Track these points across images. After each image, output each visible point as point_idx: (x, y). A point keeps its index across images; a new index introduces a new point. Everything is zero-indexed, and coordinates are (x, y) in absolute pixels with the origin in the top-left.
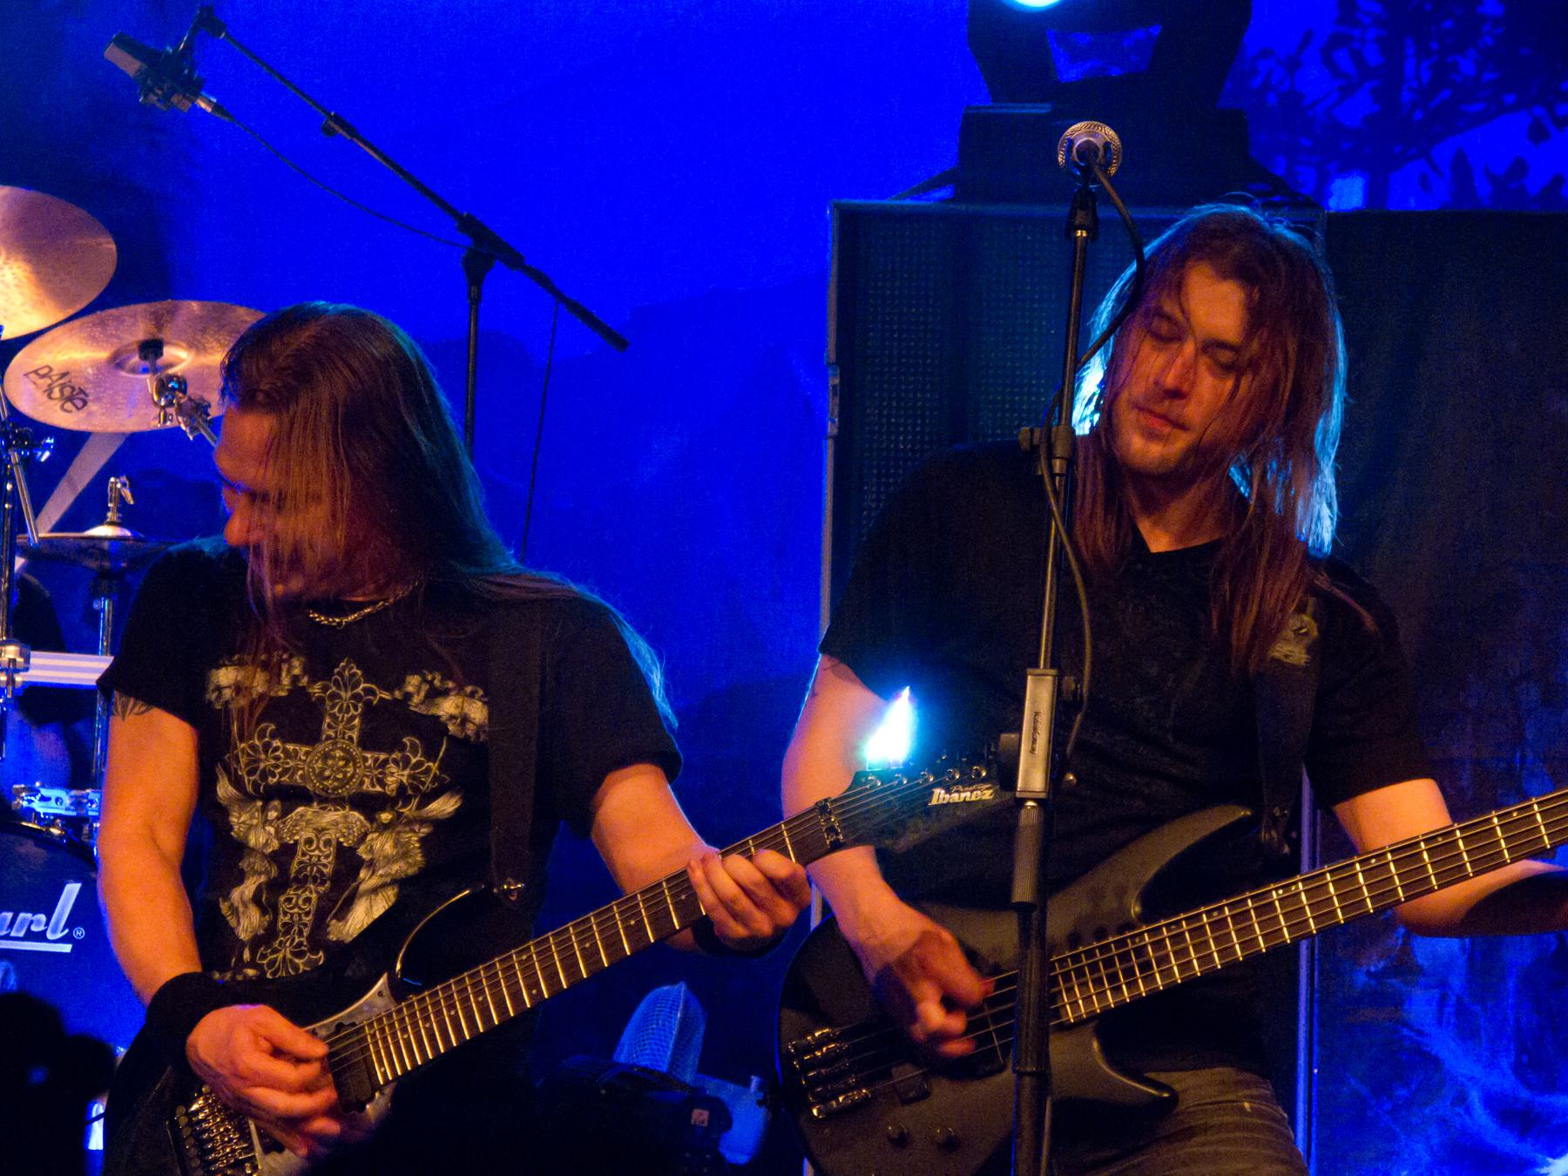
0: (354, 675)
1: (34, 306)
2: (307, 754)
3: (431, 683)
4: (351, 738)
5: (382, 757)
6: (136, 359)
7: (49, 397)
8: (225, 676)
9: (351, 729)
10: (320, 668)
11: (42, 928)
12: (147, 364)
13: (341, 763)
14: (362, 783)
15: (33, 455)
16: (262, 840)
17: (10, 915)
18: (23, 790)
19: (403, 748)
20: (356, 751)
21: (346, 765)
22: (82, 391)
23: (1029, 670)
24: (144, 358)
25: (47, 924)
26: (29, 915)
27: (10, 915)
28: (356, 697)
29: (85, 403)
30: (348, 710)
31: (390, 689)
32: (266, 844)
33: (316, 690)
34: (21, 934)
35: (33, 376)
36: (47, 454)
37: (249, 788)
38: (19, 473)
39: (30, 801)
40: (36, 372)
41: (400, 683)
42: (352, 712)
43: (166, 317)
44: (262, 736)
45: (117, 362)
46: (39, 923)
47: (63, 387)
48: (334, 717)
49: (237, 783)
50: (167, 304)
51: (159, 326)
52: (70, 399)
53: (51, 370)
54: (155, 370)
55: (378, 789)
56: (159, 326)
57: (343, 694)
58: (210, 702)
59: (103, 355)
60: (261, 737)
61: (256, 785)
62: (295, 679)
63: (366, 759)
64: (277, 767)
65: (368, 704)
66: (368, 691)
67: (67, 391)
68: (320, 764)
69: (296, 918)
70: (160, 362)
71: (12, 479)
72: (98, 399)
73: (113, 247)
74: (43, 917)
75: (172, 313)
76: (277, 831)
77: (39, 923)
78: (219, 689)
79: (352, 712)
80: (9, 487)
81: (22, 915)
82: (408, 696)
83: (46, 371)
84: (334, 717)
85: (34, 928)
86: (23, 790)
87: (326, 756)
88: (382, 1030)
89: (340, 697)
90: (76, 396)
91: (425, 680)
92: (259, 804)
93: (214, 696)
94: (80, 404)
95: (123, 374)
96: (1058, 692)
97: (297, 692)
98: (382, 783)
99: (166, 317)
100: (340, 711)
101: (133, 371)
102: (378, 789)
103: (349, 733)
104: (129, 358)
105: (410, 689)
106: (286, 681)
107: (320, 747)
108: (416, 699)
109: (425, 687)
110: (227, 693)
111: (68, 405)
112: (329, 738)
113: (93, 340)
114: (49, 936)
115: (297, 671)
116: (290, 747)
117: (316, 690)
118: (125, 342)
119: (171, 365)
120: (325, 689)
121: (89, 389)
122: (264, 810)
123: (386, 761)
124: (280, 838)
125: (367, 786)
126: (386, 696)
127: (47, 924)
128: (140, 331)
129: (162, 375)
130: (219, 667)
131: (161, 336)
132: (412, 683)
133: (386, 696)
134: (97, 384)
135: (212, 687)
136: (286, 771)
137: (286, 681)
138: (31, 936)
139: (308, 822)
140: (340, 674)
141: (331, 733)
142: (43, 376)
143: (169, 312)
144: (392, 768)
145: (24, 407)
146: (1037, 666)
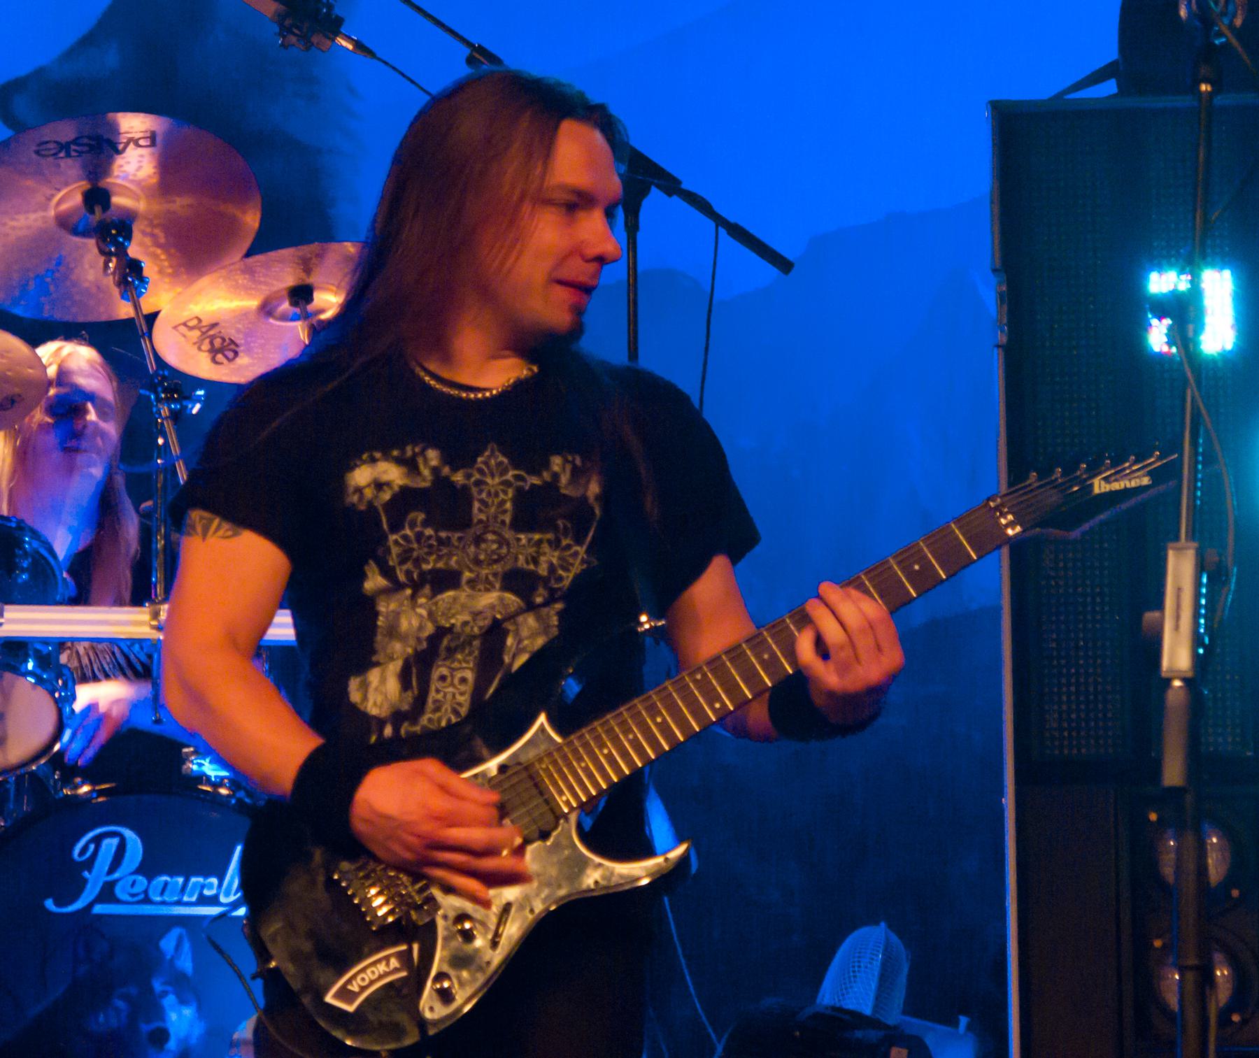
0: (501, 463)
1: (175, 275)
2: (460, 539)
3: (573, 462)
4: (503, 522)
5: (537, 537)
6: (286, 306)
7: (199, 349)
8: (361, 476)
9: (505, 512)
10: (458, 456)
11: (213, 892)
12: (298, 310)
13: (495, 546)
14: (516, 559)
15: (184, 408)
16: (415, 623)
17: (181, 880)
18: (193, 753)
19: (555, 529)
20: (508, 534)
21: (500, 547)
22: (232, 341)
23: (1171, 545)
24: (294, 303)
25: (220, 885)
26: (201, 880)
27: (181, 880)
28: (507, 484)
29: (236, 354)
30: (497, 495)
31: (539, 474)
32: (421, 628)
33: (458, 478)
34: (194, 899)
35: (182, 329)
36: (198, 406)
37: (402, 577)
38: (169, 426)
39: (200, 765)
40: (185, 324)
41: (546, 465)
42: (502, 496)
43: (314, 260)
44: (413, 525)
45: (266, 309)
46: (210, 886)
47: (212, 338)
48: (482, 502)
49: (387, 572)
50: (315, 247)
51: (308, 271)
52: (221, 350)
53: (200, 320)
54: (306, 316)
55: (532, 567)
56: (307, 267)
57: (489, 480)
58: (354, 505)
59: (253, 303)
60: (412, 528)
61: (408, 573)
62: (435, 471)
63: (519, 540)
64: (430, 554)
65: (519, 491)
66: (518, 477)
67: (218, 342)
68: (472, 549)
69: (449, 697)
70: (310, 308)
71: (163, 433)
72: (249, 351)
73: (257, 225)
74: (214, 881)
75: (320, 256)
76: (430, 614)
77: (210, 886)
78: (359, 490)
79: (502, 496)
80: (160, 441)
81: (193, 880)
82: (556, 476)
83: (195, 322)
84: (482, 502)
85: (207, 892)
86: (193, 753)
87: (478, 540)
88: (555, 763)
89: (487, 484)
90: (223, 348)
91: (566, 461)
92: (409, 592)
93: (355, 498)
94: (231, 355)
95: (271, 320)
96: (1201, 567)
97: (440, 481)
98: (535, 561)
99: (314, 260)
100: (489, 494)
101: (284, 318)
102: (532, 567)
103: (501, 517)
104: (279, 305)
105: (556, 468)
106: (426, 472)
107: (472, 532)
108: (564, 479)
109: (569, 467)
110: (369, 493)
111: (220, 357)
112: (480, 521)
113: (237, 289)
114: (223, 899)
115: (434, 463)
116: (443, 534)
117: (458, 478)
118: (275, 289)
119: (322, 311)
120: (468, 476)
121: (239, 339)
122: (413, 597)
123: (540, 542)
124: (434, 621)
125: (521, 562)
126: (535, 481)
127: (220, 885)
128: (289, 279)
129: (314, 321)
130: (352, 469)
131: (312, 280)
132: (556, 462)
133: (535, 481)
134: (249, 334)
135: (351, 490)
136: (440, 558)
137: (426, 472)
138: (203, 901)
139: (463, 606)
140: (486, 463)
141: (483, 517)
142: (191, 328)
143: (318, 256)
144: (546, 548)
145: (171, 358)
146: (1177, 538)
